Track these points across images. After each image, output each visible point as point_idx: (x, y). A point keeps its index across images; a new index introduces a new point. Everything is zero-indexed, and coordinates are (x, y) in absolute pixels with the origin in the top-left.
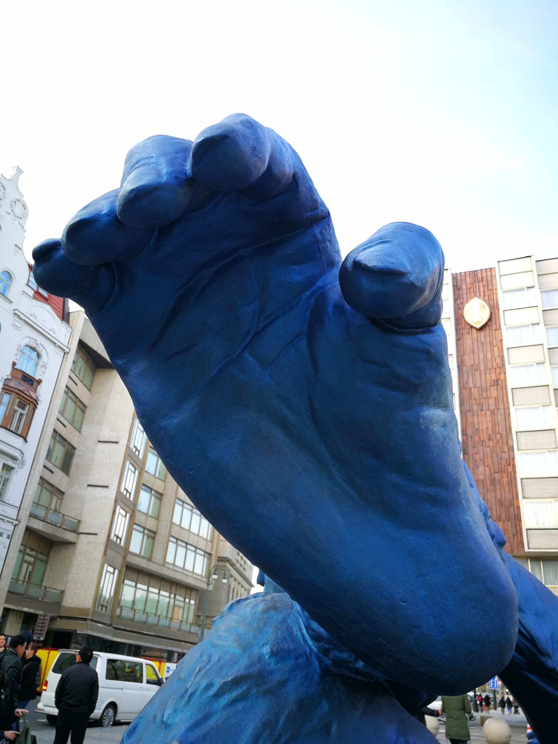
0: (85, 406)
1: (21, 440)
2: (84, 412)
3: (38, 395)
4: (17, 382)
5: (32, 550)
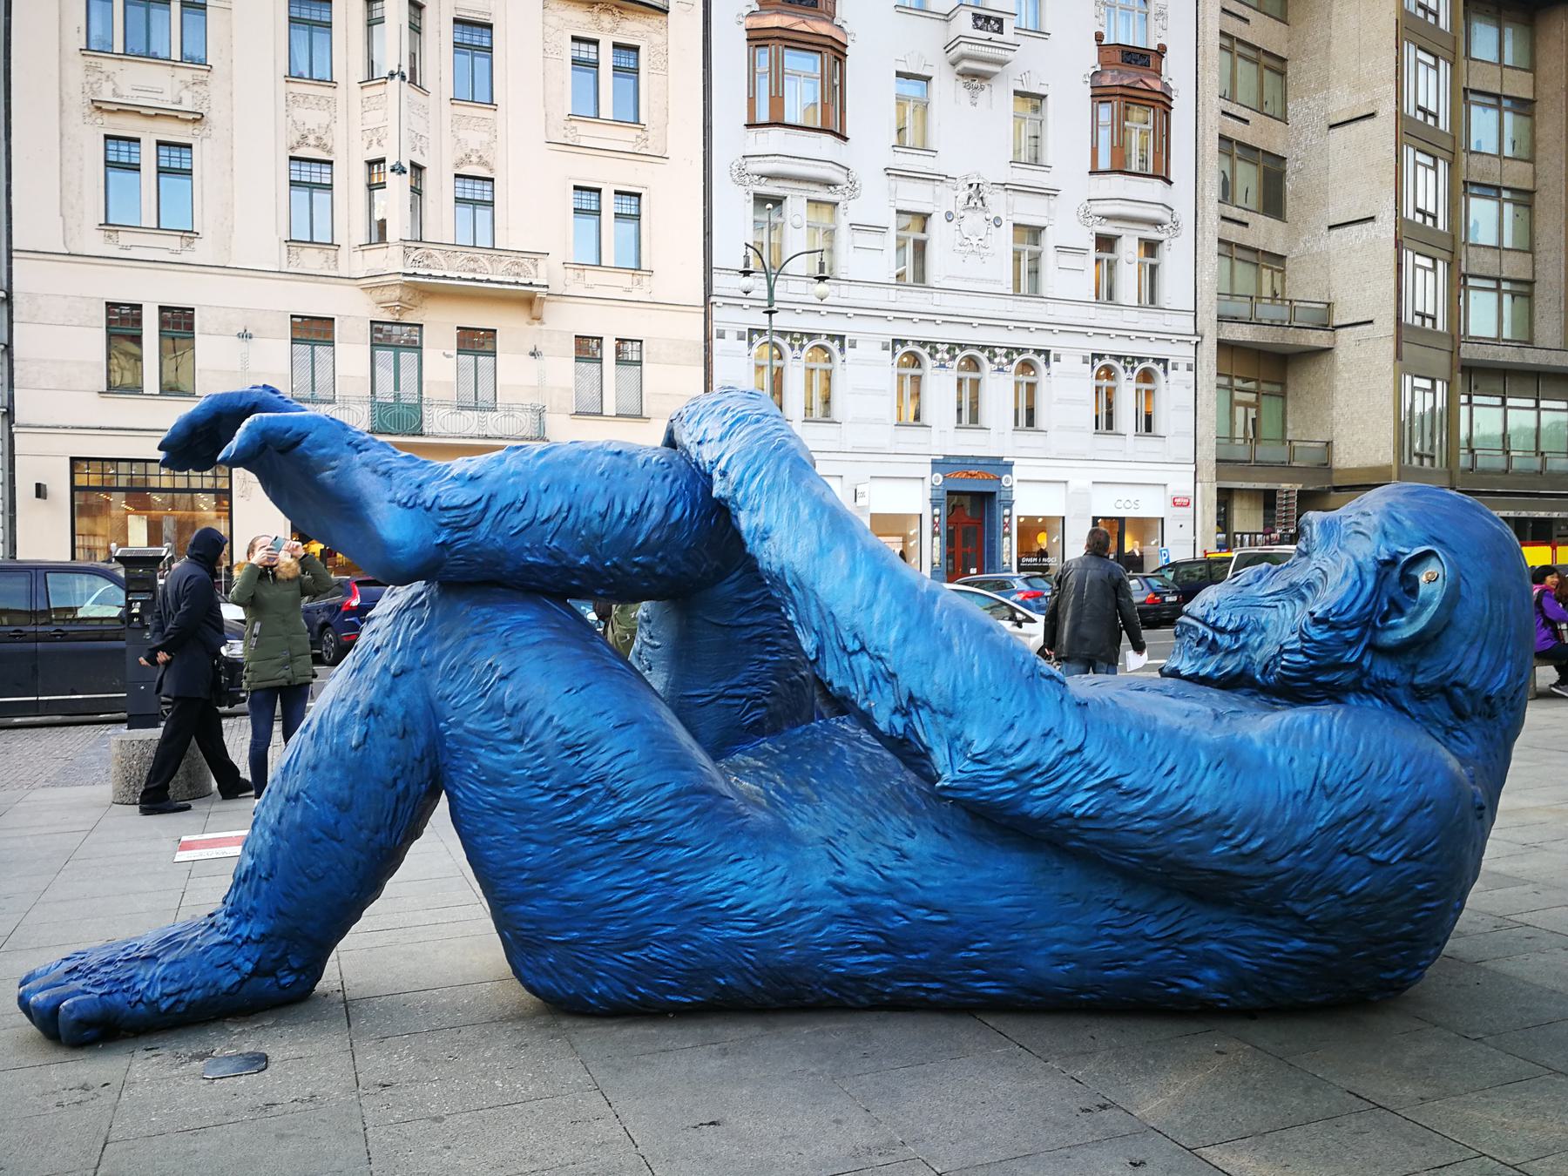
0: (1283, 60)
1: (1159, 183)
2: (1283, 74)
3: (1164, 79)
4: (1116, 73)
5: (1247, 380)
